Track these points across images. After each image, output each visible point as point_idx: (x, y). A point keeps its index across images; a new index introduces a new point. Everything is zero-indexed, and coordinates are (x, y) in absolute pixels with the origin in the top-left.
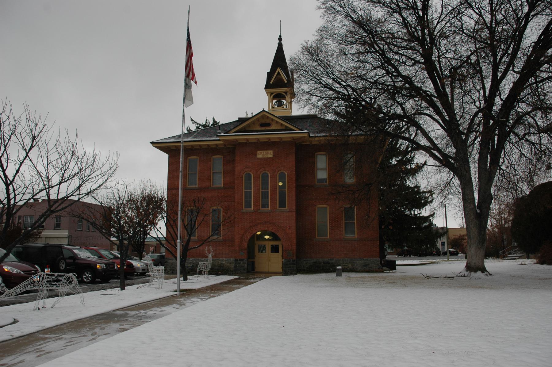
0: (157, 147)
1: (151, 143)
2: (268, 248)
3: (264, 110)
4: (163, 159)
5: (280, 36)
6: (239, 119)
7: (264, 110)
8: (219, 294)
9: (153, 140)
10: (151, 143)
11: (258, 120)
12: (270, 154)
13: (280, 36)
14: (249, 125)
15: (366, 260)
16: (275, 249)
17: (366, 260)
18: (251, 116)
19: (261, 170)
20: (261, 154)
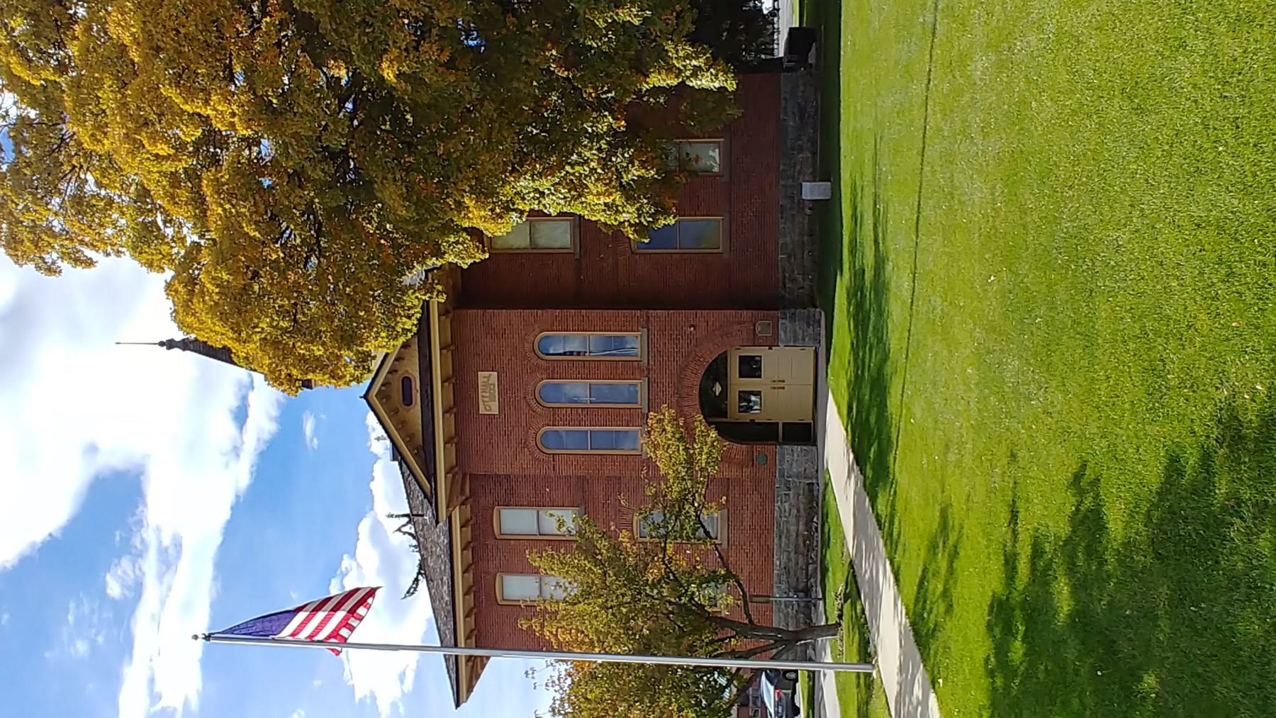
0: (470, 689)
1: (458, 705)
2: (749, 384)
3: (365, 397)
4: (503, 668)
5: (162, 344)
6: (394, 459)
7: (365, 397)
8: (252, 473)
9: (453, 705)
10: (458, 705)
11: (393, 413)
12: (488, 380)
13: (162, 344)
14: (409, 439)
15: (786, 114)
16: (751, 367)
17: (786, 114)
18: (388, 442)
19: (533, 403)
20: (489, 404)
